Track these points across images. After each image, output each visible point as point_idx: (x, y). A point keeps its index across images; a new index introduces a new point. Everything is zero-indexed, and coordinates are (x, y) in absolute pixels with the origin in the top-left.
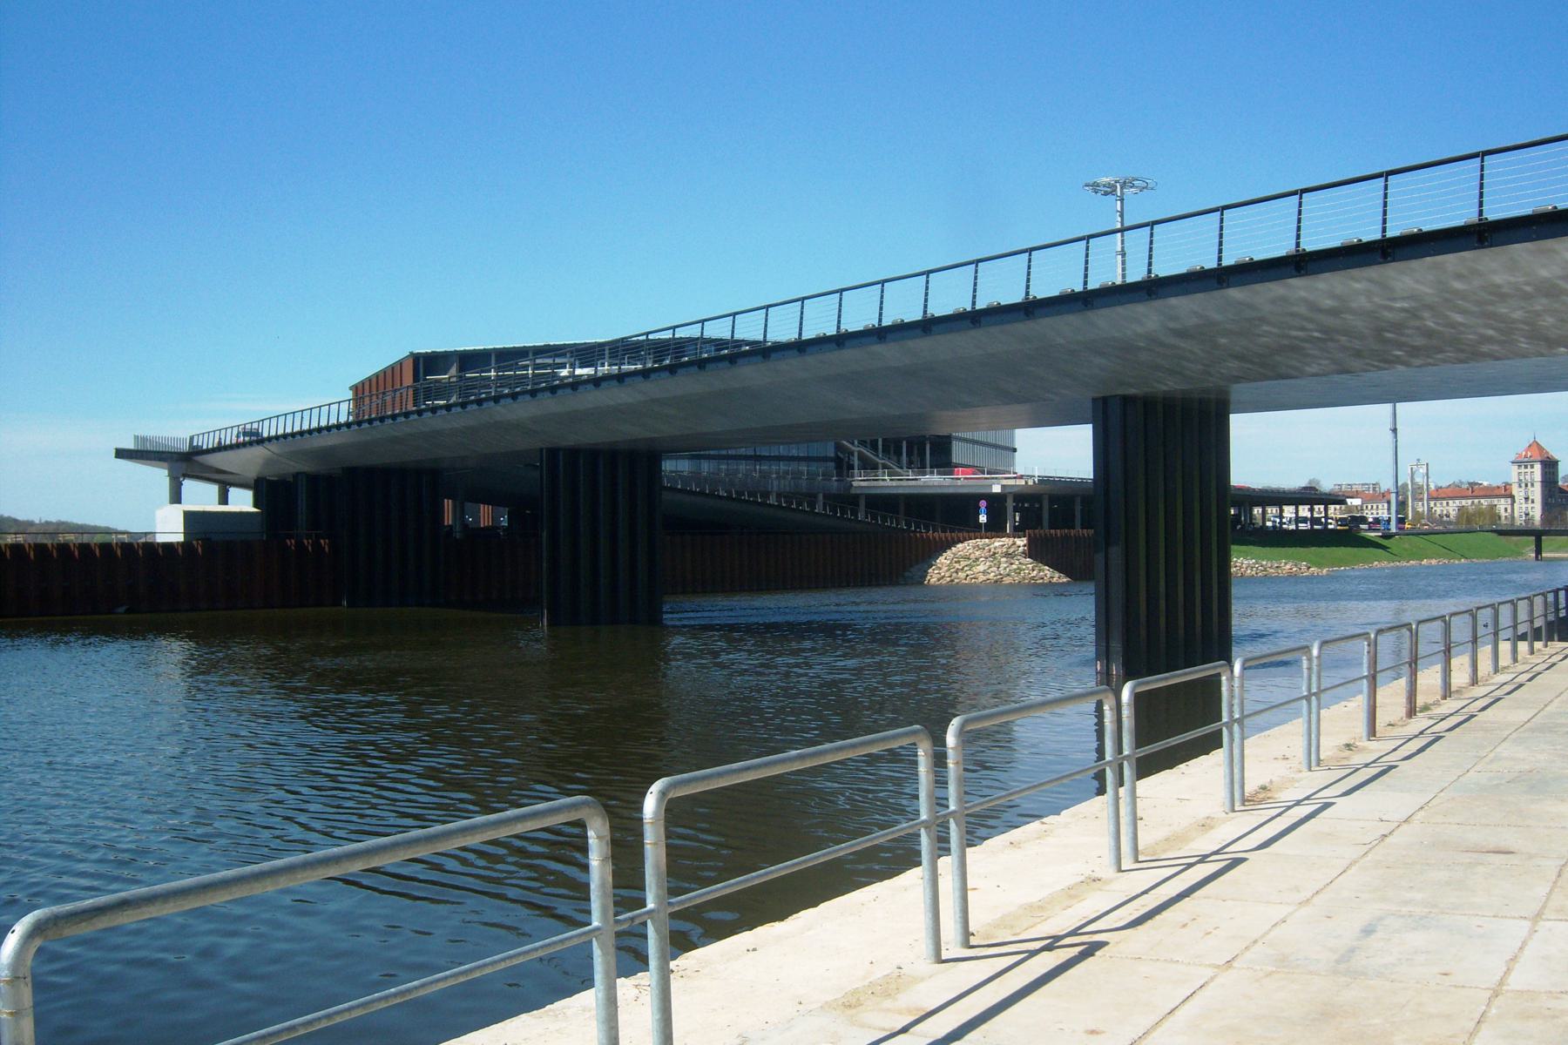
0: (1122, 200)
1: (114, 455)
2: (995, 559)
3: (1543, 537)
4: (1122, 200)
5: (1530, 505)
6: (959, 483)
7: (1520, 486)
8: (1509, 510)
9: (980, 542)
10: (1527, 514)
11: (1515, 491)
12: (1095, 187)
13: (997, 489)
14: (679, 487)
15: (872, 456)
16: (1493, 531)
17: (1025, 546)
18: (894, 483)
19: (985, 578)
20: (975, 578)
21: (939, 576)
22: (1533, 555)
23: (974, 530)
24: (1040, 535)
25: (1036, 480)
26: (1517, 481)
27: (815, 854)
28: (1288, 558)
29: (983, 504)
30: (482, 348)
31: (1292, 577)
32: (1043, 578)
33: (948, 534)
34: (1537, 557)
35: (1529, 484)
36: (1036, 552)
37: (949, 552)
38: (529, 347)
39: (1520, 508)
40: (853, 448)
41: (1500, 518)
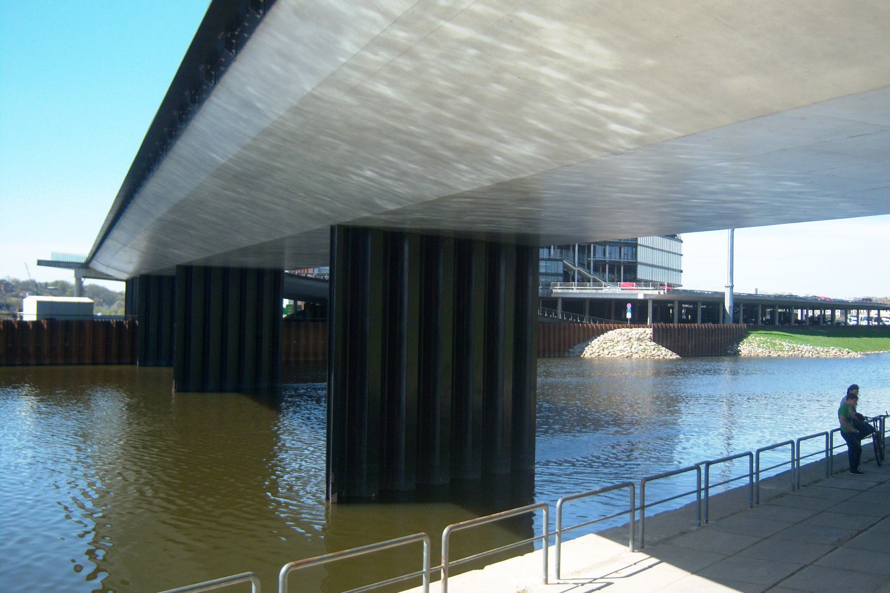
1: (36, 264)
9: (623, 330)
13: (641, 296)
15: (586, 273)
17: (651, 334)
18: (578, 291)
19: (621, 354)
21: (591, 352)
24: (698, 327)
27: (520, 508)
28: (836, 345)
29: (629, 306)
31: (836, 359)
32: (659, 356)
36: (659, 338)
40: (575, 268)
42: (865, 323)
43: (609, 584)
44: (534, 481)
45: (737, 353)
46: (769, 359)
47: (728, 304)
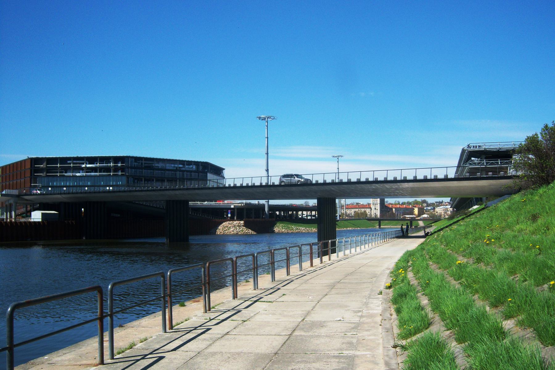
0: (267, 122)
2: (235, 227)
3: (381, 221)
4: (267, 122)
5: (376, 211)
6: (221, 205)
7: (373, 205)
8: (370, 212)
10: (375, 214)
11: (372, 206)
12: (260, 118)
14: (151, 205)
16: (366, 219)
17: (243, 223)
19: (233, 233)
20: (230, 233)
22: (378, 227)
23: (226, 220)
25: (244, 204)
26: (372, 203)
29: (229, 211)
30: (55, 157)
33: (222, 220)
34: (379, 227)
35: (376, 204)
37: (221, 225)
38: (72, 157)
39: (373, 212)
41: (367, 214)
42: (309, 218)
43: (161, 358)
44: (103, 307)
45: (273, 232)
46: (288, 234)
47: (266, 209)
